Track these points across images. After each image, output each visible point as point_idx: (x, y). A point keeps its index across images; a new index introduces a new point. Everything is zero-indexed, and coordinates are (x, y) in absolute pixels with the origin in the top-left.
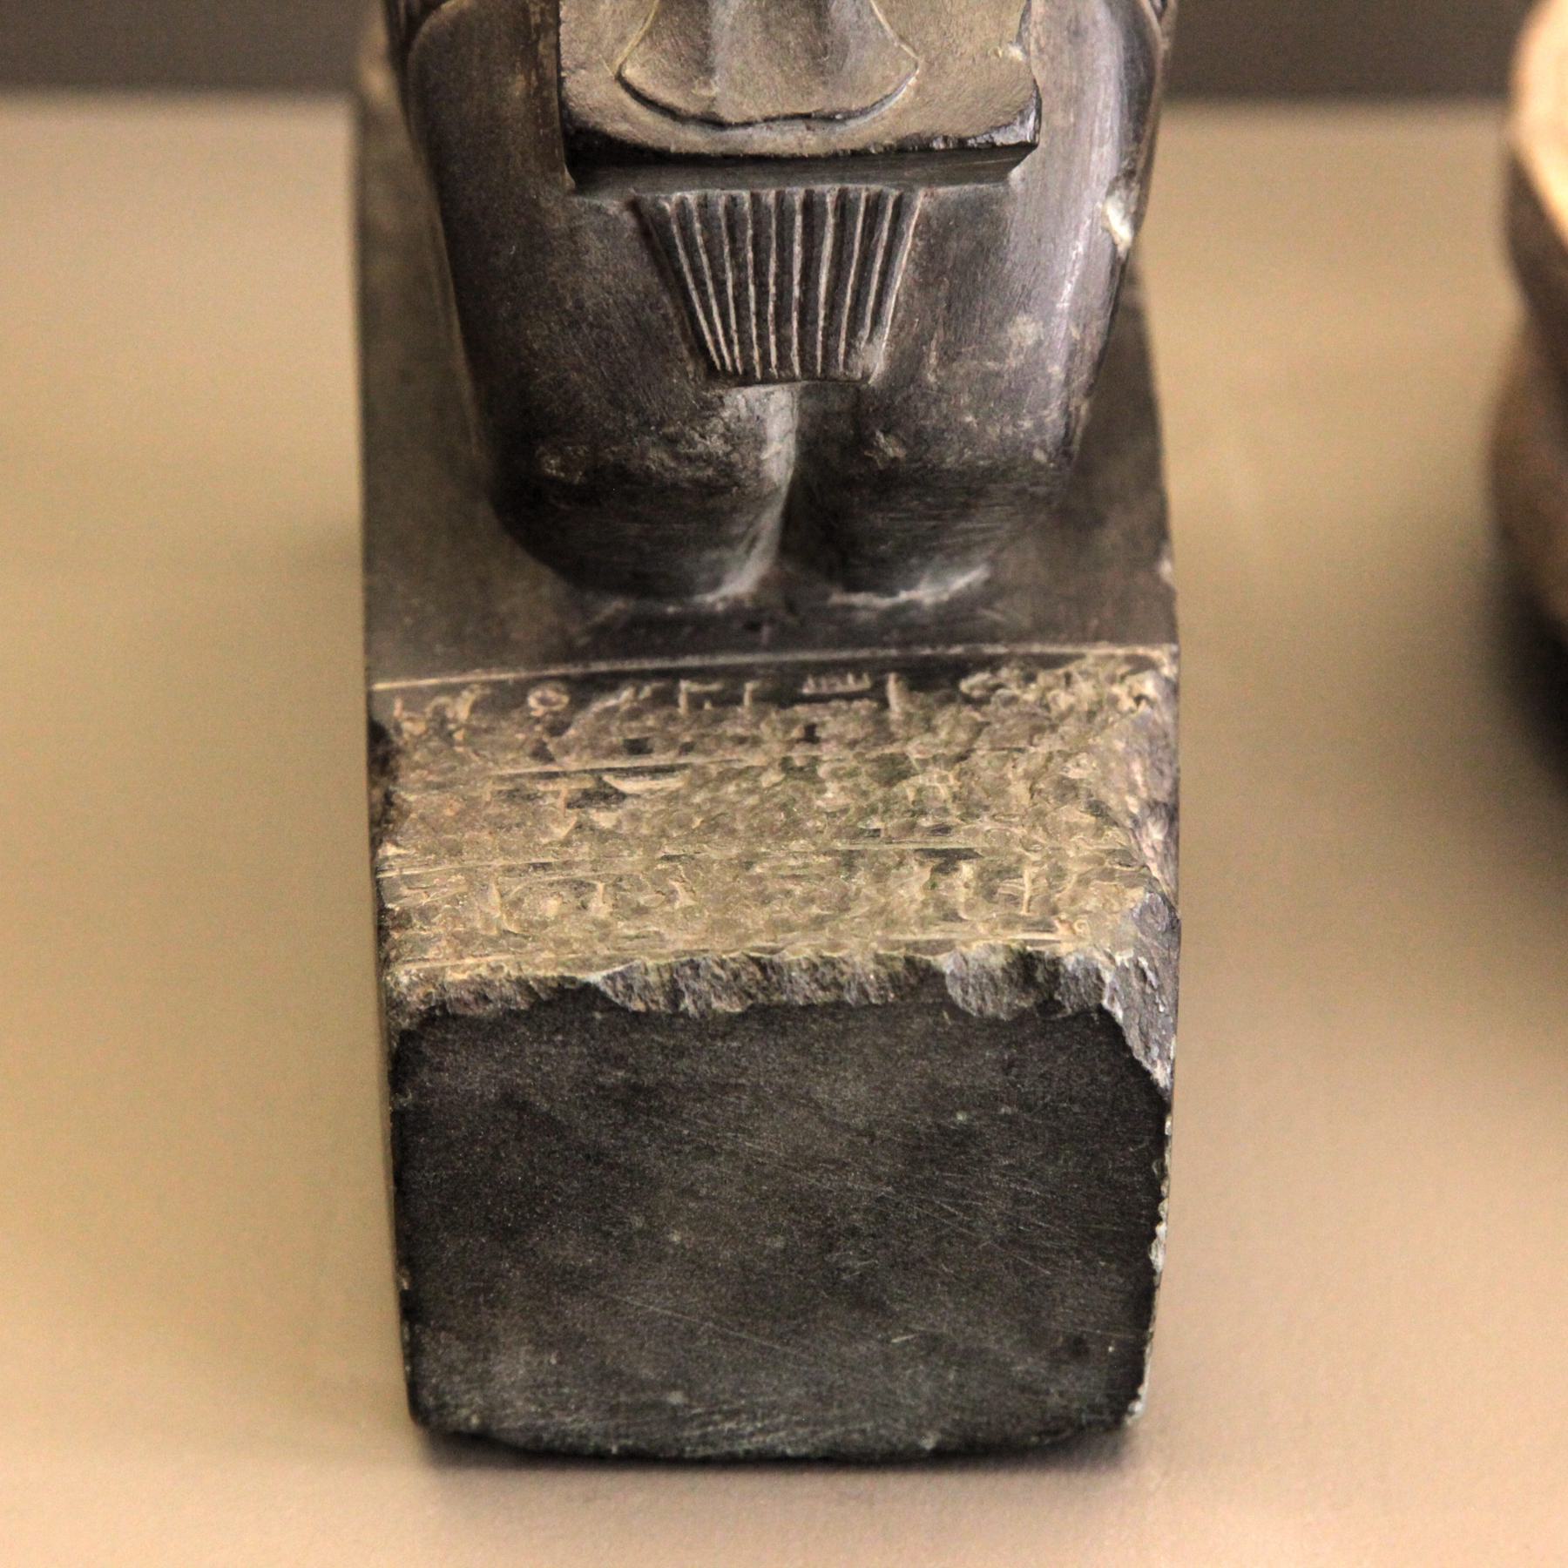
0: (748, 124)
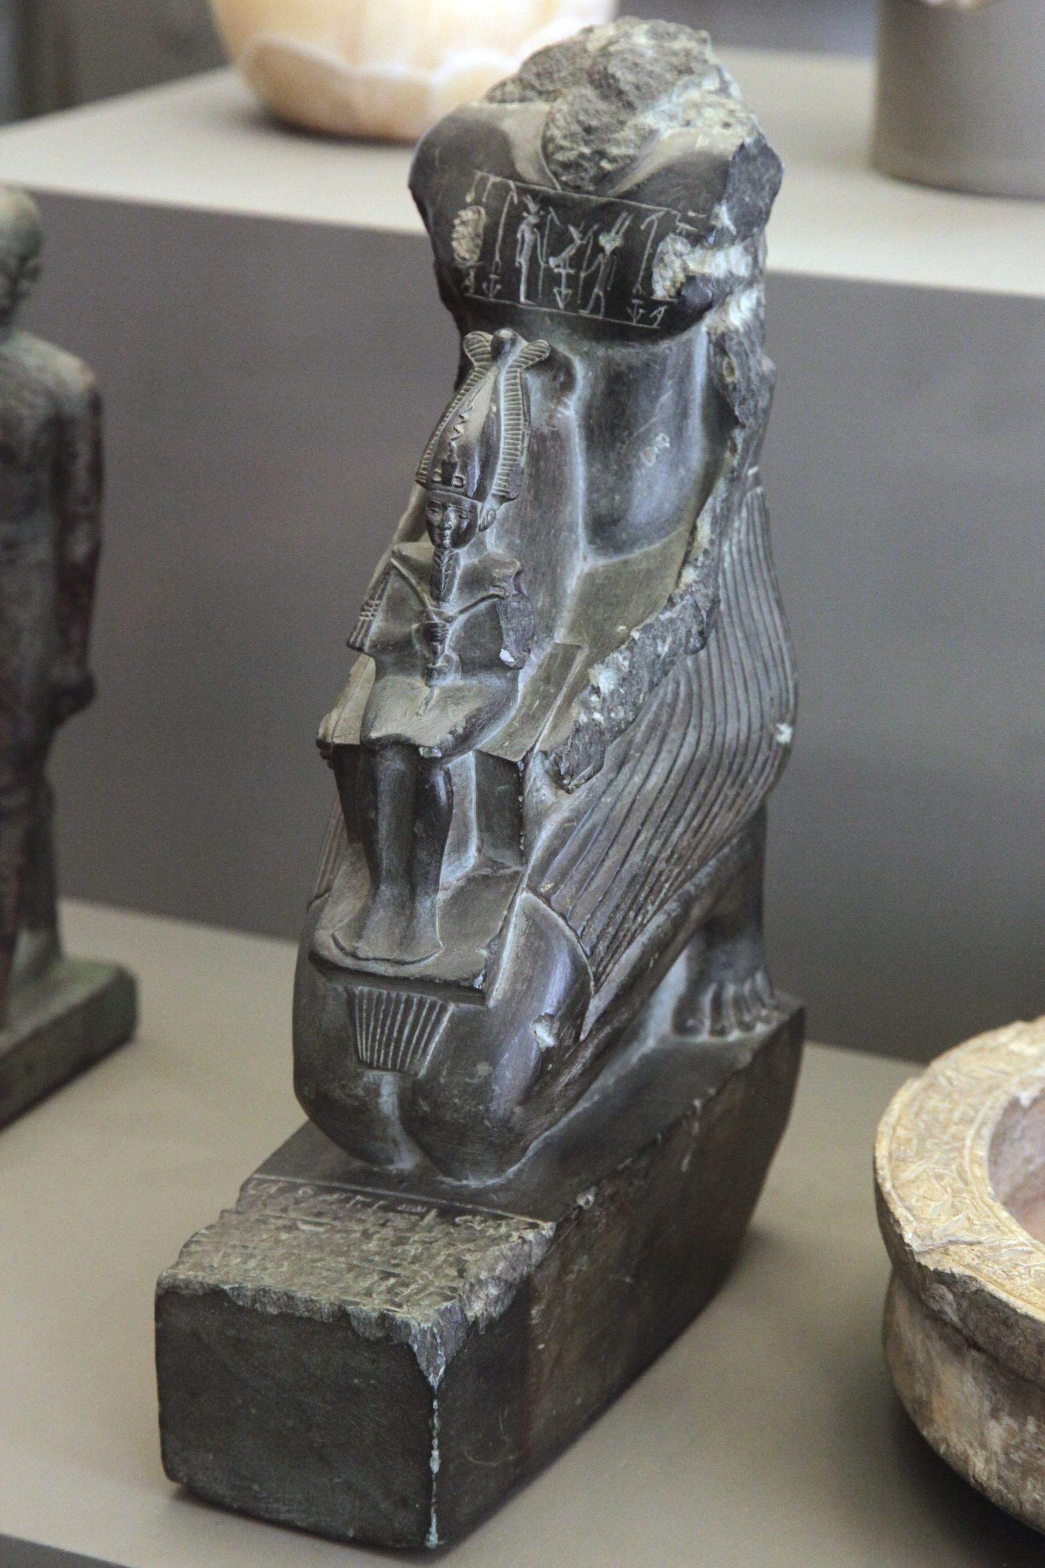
0: (367, 959)
